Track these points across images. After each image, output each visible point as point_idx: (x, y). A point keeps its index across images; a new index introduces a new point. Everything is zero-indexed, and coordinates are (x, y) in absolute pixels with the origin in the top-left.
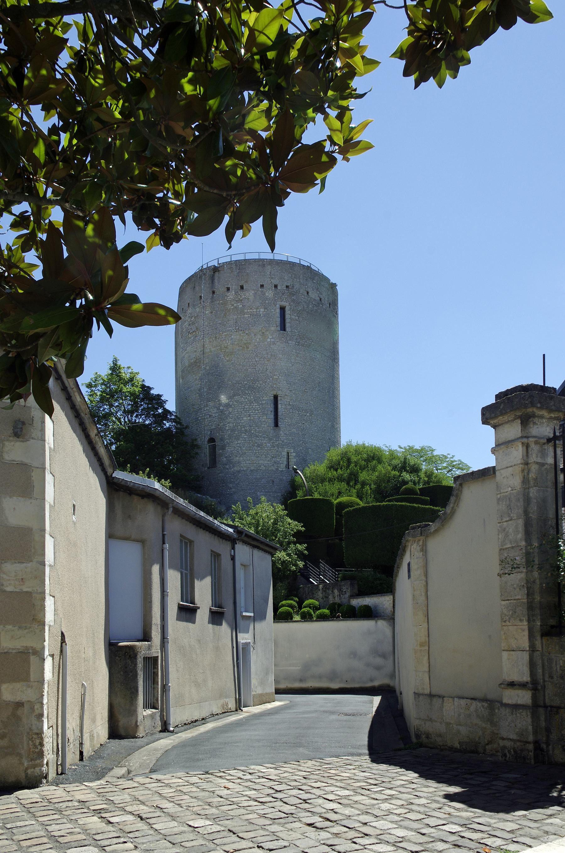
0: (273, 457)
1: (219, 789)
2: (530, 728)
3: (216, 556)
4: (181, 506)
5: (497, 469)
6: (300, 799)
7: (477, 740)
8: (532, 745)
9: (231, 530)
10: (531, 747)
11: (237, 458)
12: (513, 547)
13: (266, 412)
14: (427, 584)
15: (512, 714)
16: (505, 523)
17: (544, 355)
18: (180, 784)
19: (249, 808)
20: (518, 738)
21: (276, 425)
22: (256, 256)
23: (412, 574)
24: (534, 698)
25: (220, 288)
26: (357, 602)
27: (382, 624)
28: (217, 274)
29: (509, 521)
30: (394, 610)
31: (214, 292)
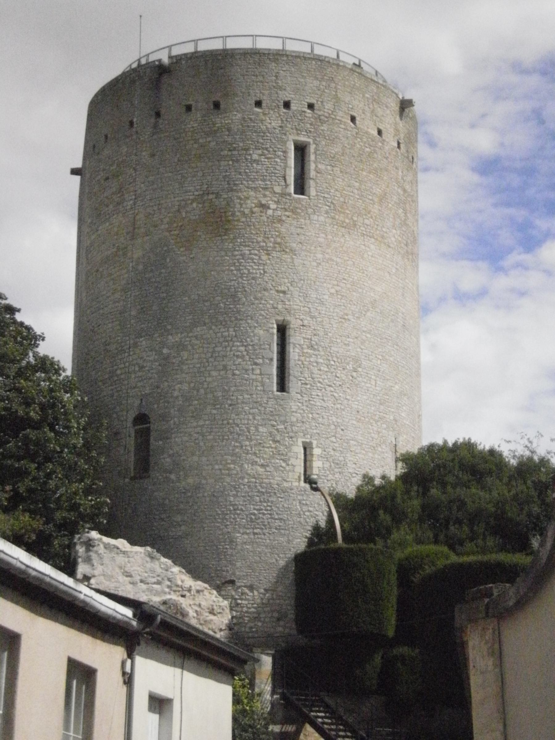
3: (81, 675)
11: (196, 458)
28: (165, 78)
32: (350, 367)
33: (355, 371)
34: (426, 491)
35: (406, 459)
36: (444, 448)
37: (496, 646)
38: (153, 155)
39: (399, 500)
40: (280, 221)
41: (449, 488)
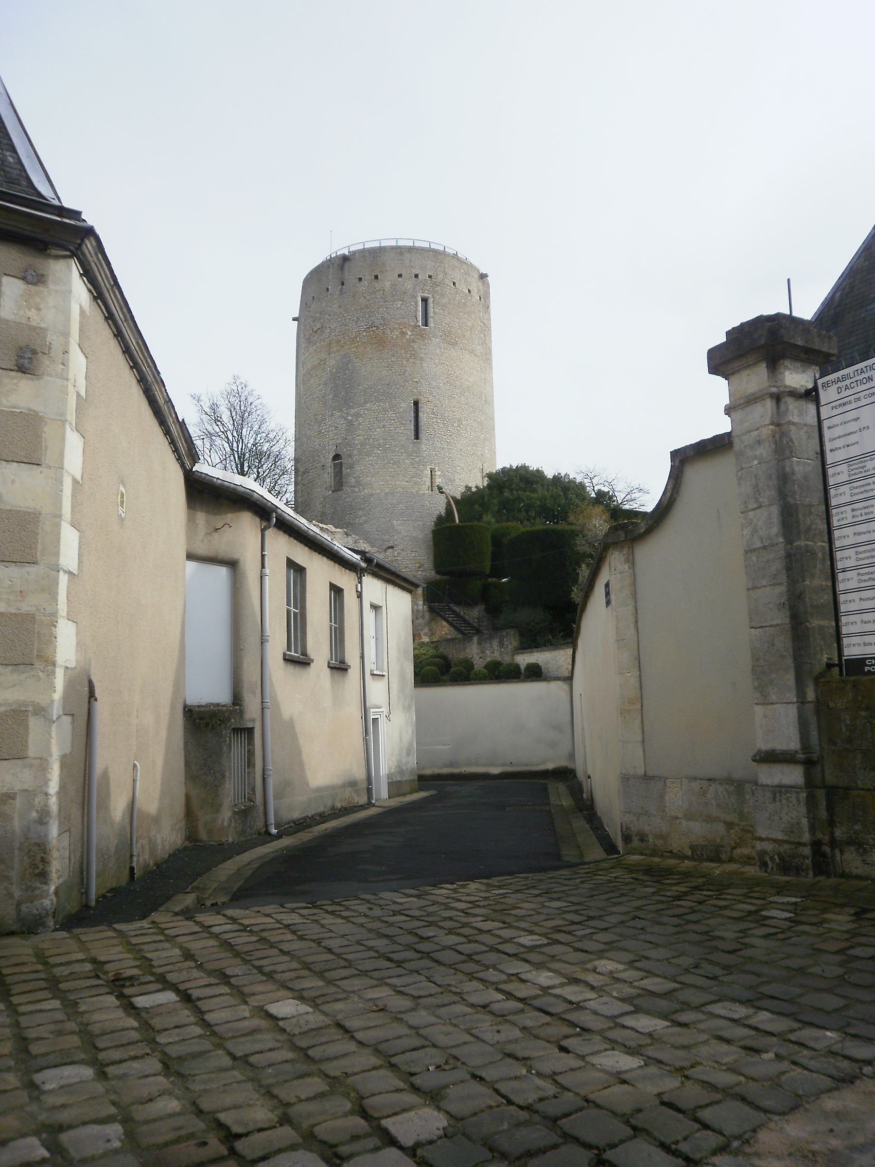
1: (329, 935)
2: (805, 822)
4: (288, 517)
5: (734, 434)
6: (461, 953)
7: (718, 841)
8: (809, 847)
9: (358, 557)
10: (807, 851)
12: (765, 548)
14: (636, 610)
15: (774, 800)
16: (751, 513)
17: (789, 280)
18: (269, 926)
19: (376, 974)
20: (786, 838)
22: (393, 243)
23: (613, 597)
24: (808, 776)
25: (350, 278)
26: (524, 660)
27: (557, 689)
29: (756, 508)
30: (573, 668)
31: (343, 284)
32: (456, 425)
33: (459, 426)
34: (501, 493)
35: (490, 476)
36: (511, 469)
37: (631, 557)
38: (340, 307)
39: (486, 499)
40: (414, 341)
41: (514, 492)
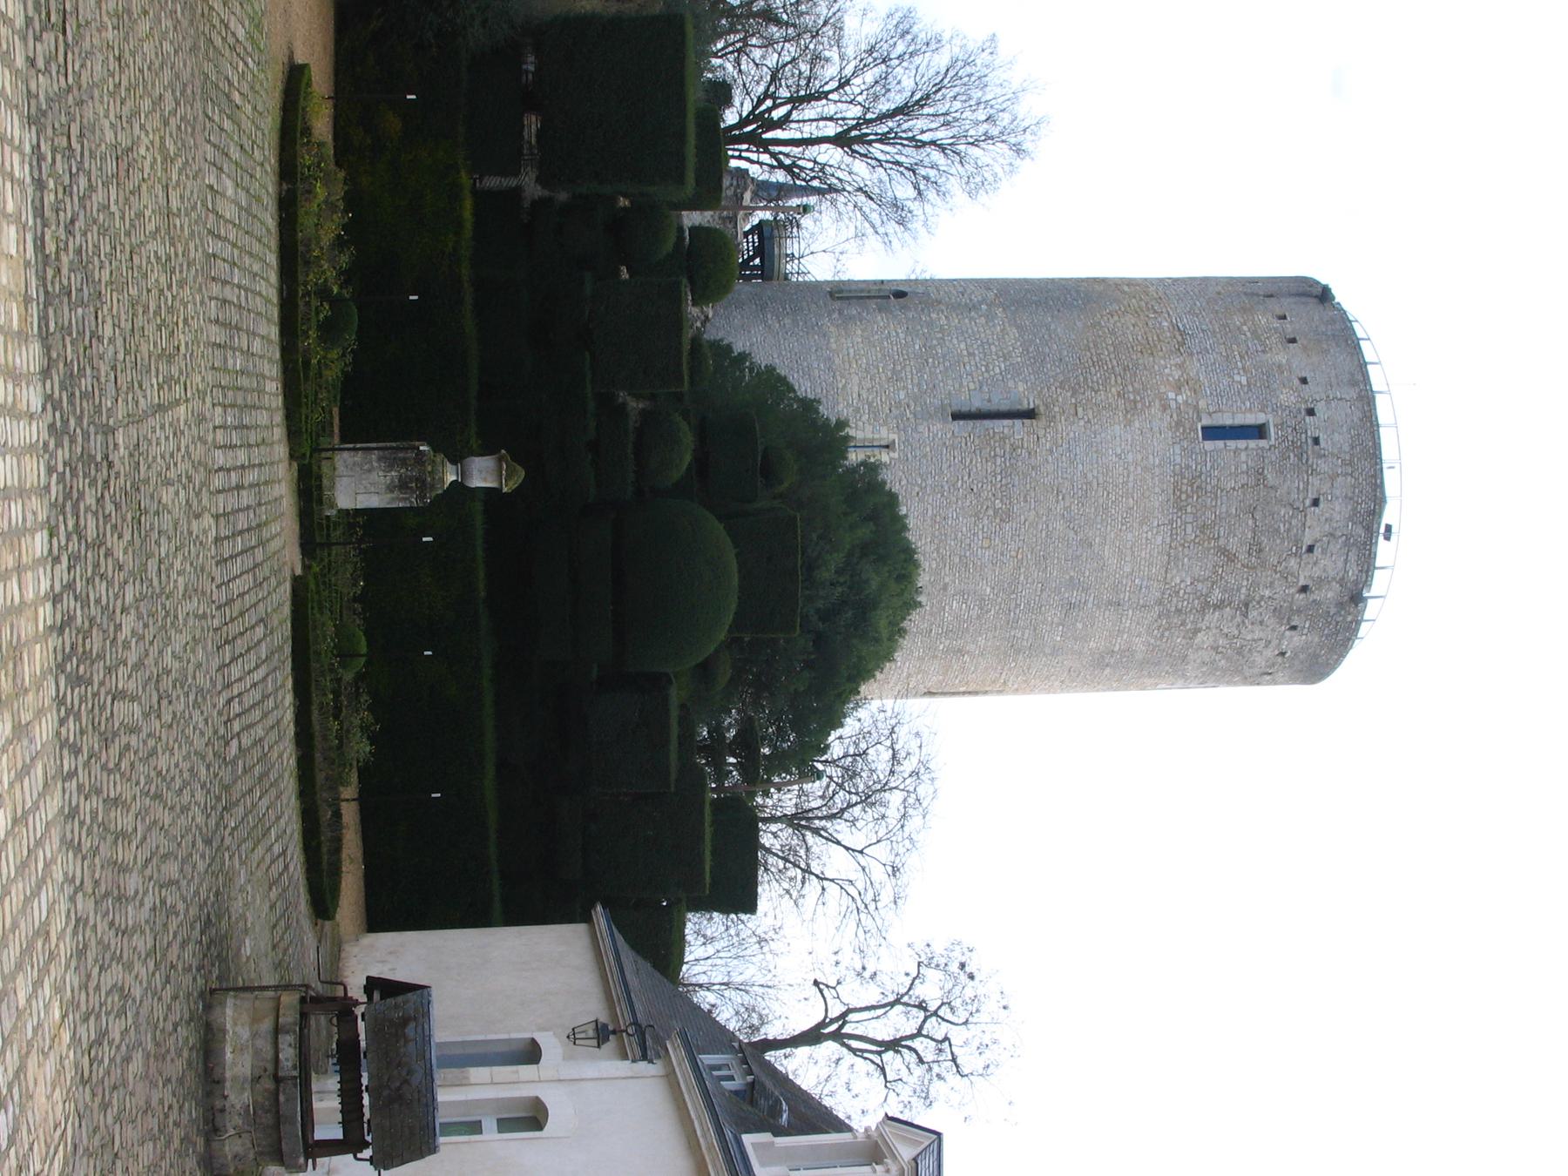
0: (870, 405)
13: (985, 389)
21: (957, 416)
